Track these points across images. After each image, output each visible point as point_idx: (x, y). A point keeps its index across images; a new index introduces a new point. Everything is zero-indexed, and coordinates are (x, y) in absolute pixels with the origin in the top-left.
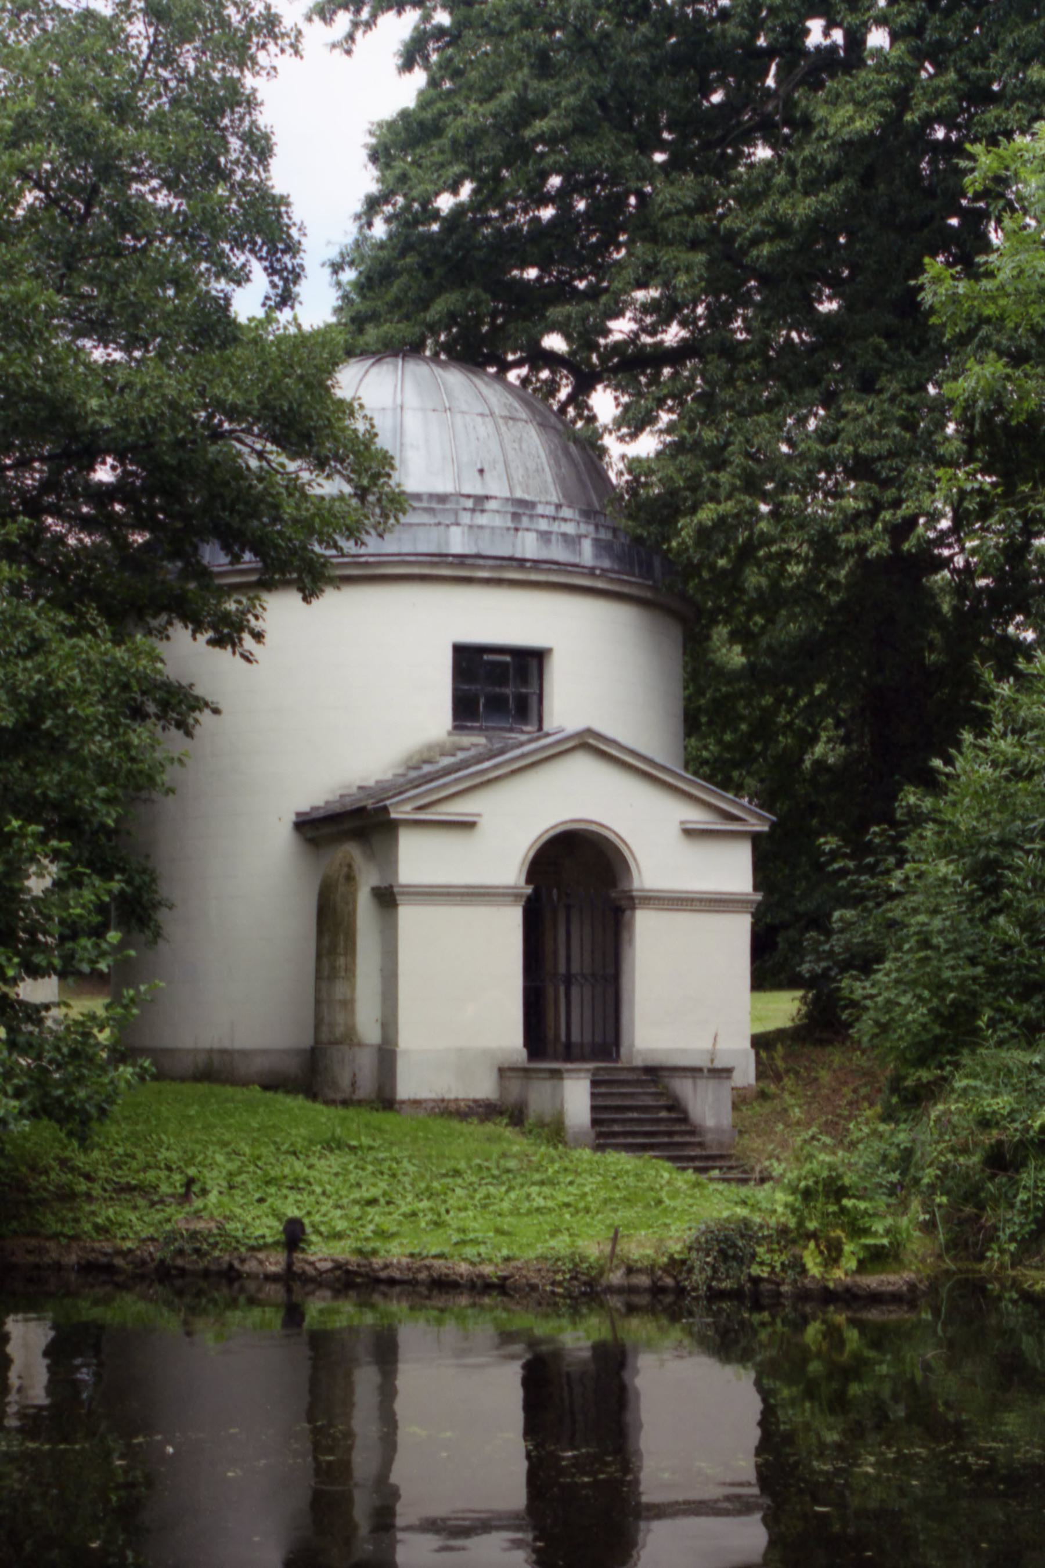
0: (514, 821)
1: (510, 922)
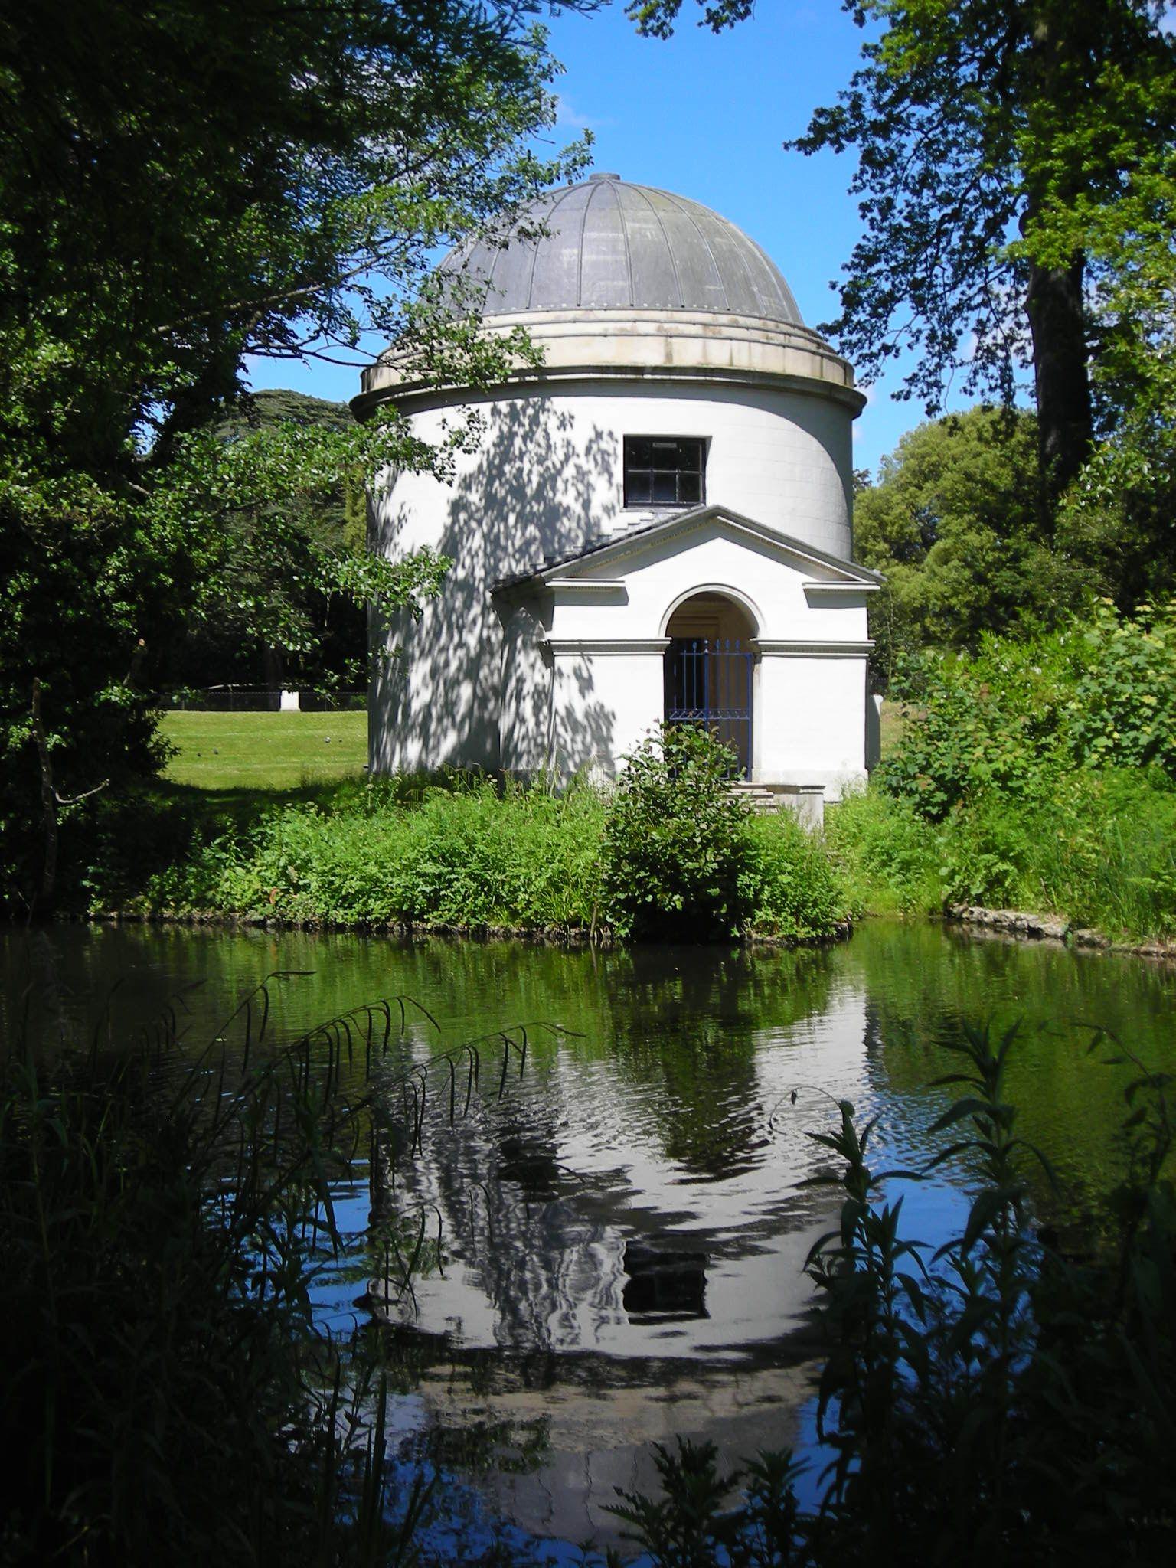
0: (654, 594)
1: (655, 665)
